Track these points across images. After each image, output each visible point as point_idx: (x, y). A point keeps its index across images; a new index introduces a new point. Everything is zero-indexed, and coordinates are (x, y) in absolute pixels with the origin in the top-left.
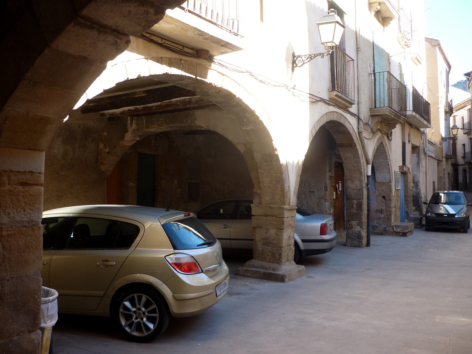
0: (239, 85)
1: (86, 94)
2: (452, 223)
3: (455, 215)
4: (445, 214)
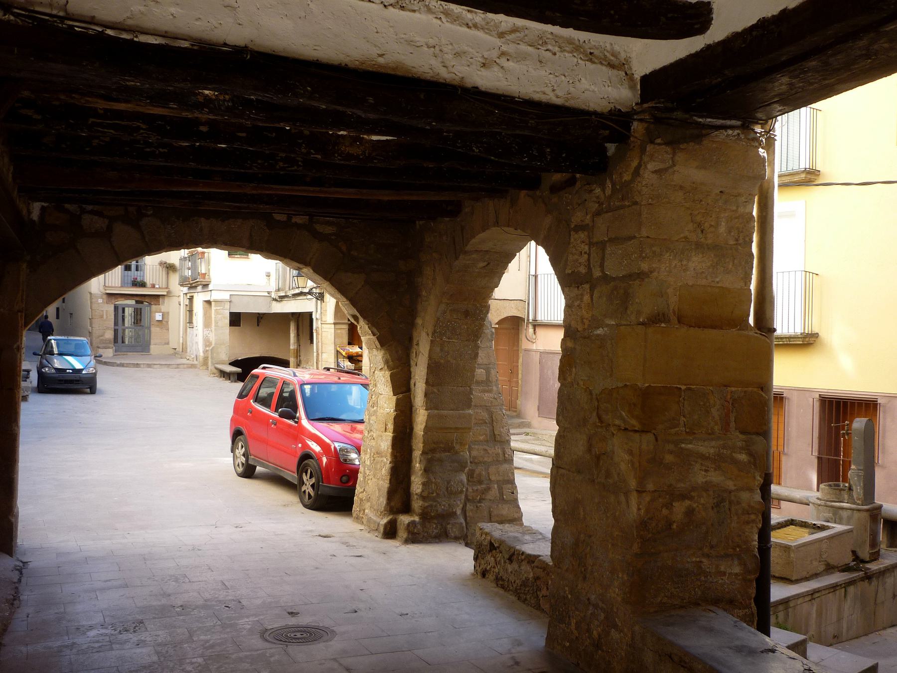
0: (832, 562)
1: (98, 279)
2: (78, 381)
3: (82, 370)
4: (69, 369)
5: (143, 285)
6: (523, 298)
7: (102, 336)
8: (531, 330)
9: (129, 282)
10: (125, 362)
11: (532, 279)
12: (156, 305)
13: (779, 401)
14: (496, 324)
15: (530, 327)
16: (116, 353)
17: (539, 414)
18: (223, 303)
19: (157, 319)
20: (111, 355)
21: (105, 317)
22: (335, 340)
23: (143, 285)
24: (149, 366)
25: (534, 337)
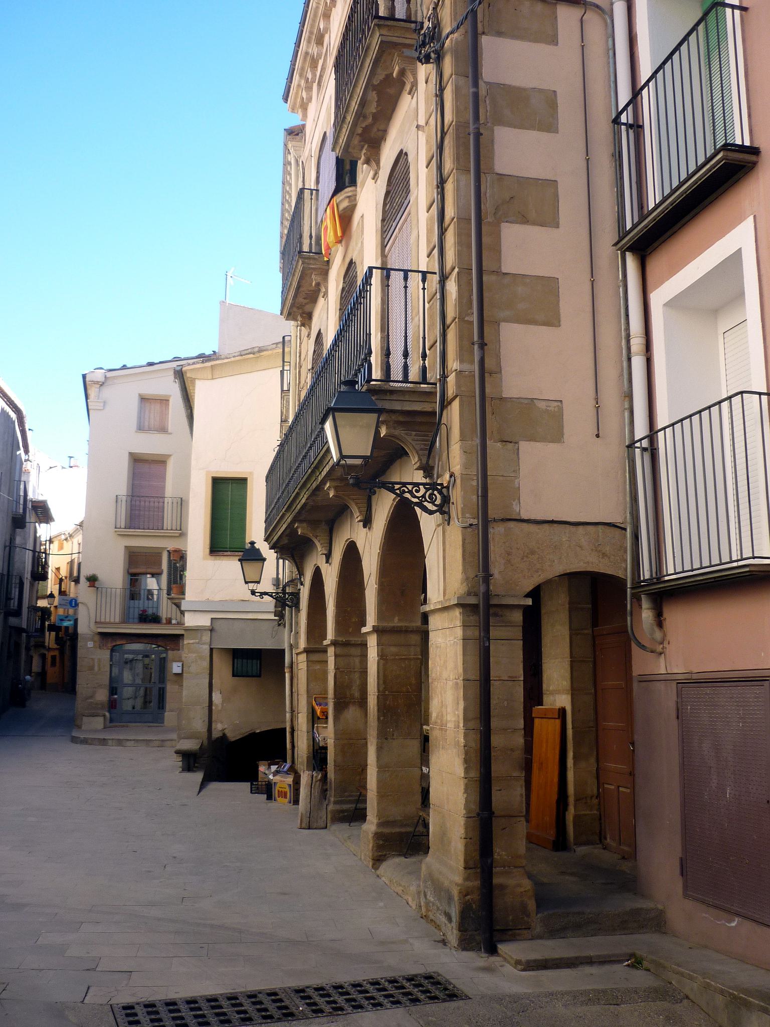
5: (156, 620)
6: (616, 519)
7: (91, 697)
8: (647, 614)
9: (136, 615)
10: (91, 737)
11: (641, 461)
12: (173, 650)
13: (526, 756)
14: (527, 596)
15: (646, 604)
16: (111, 724)
17: (685, 887)
18: (199, 631)
19: (174, 672)
20: (101, 726)
21: (96, 668)
22: (307, 687)
23: (156, 620)
24: (120, 742)
25: (658, 635)
